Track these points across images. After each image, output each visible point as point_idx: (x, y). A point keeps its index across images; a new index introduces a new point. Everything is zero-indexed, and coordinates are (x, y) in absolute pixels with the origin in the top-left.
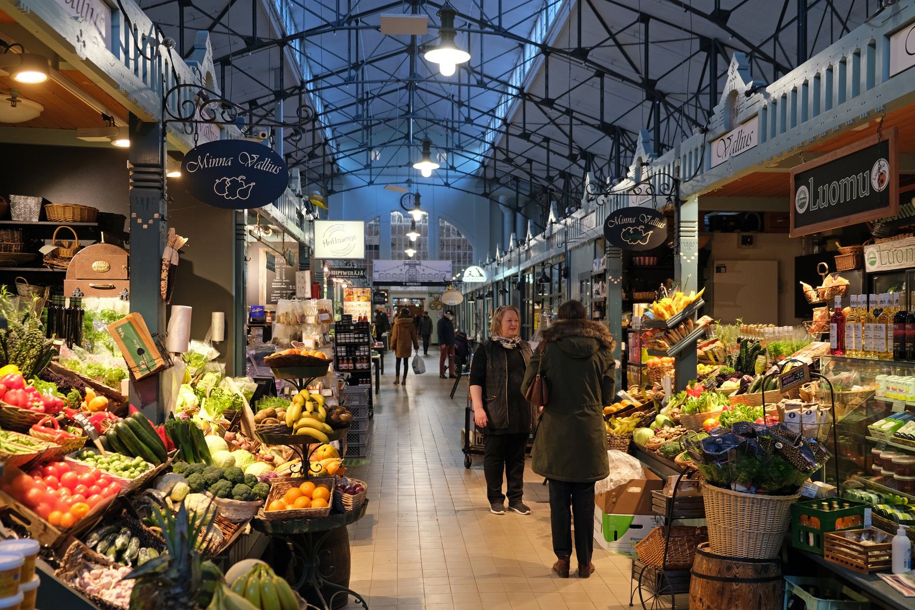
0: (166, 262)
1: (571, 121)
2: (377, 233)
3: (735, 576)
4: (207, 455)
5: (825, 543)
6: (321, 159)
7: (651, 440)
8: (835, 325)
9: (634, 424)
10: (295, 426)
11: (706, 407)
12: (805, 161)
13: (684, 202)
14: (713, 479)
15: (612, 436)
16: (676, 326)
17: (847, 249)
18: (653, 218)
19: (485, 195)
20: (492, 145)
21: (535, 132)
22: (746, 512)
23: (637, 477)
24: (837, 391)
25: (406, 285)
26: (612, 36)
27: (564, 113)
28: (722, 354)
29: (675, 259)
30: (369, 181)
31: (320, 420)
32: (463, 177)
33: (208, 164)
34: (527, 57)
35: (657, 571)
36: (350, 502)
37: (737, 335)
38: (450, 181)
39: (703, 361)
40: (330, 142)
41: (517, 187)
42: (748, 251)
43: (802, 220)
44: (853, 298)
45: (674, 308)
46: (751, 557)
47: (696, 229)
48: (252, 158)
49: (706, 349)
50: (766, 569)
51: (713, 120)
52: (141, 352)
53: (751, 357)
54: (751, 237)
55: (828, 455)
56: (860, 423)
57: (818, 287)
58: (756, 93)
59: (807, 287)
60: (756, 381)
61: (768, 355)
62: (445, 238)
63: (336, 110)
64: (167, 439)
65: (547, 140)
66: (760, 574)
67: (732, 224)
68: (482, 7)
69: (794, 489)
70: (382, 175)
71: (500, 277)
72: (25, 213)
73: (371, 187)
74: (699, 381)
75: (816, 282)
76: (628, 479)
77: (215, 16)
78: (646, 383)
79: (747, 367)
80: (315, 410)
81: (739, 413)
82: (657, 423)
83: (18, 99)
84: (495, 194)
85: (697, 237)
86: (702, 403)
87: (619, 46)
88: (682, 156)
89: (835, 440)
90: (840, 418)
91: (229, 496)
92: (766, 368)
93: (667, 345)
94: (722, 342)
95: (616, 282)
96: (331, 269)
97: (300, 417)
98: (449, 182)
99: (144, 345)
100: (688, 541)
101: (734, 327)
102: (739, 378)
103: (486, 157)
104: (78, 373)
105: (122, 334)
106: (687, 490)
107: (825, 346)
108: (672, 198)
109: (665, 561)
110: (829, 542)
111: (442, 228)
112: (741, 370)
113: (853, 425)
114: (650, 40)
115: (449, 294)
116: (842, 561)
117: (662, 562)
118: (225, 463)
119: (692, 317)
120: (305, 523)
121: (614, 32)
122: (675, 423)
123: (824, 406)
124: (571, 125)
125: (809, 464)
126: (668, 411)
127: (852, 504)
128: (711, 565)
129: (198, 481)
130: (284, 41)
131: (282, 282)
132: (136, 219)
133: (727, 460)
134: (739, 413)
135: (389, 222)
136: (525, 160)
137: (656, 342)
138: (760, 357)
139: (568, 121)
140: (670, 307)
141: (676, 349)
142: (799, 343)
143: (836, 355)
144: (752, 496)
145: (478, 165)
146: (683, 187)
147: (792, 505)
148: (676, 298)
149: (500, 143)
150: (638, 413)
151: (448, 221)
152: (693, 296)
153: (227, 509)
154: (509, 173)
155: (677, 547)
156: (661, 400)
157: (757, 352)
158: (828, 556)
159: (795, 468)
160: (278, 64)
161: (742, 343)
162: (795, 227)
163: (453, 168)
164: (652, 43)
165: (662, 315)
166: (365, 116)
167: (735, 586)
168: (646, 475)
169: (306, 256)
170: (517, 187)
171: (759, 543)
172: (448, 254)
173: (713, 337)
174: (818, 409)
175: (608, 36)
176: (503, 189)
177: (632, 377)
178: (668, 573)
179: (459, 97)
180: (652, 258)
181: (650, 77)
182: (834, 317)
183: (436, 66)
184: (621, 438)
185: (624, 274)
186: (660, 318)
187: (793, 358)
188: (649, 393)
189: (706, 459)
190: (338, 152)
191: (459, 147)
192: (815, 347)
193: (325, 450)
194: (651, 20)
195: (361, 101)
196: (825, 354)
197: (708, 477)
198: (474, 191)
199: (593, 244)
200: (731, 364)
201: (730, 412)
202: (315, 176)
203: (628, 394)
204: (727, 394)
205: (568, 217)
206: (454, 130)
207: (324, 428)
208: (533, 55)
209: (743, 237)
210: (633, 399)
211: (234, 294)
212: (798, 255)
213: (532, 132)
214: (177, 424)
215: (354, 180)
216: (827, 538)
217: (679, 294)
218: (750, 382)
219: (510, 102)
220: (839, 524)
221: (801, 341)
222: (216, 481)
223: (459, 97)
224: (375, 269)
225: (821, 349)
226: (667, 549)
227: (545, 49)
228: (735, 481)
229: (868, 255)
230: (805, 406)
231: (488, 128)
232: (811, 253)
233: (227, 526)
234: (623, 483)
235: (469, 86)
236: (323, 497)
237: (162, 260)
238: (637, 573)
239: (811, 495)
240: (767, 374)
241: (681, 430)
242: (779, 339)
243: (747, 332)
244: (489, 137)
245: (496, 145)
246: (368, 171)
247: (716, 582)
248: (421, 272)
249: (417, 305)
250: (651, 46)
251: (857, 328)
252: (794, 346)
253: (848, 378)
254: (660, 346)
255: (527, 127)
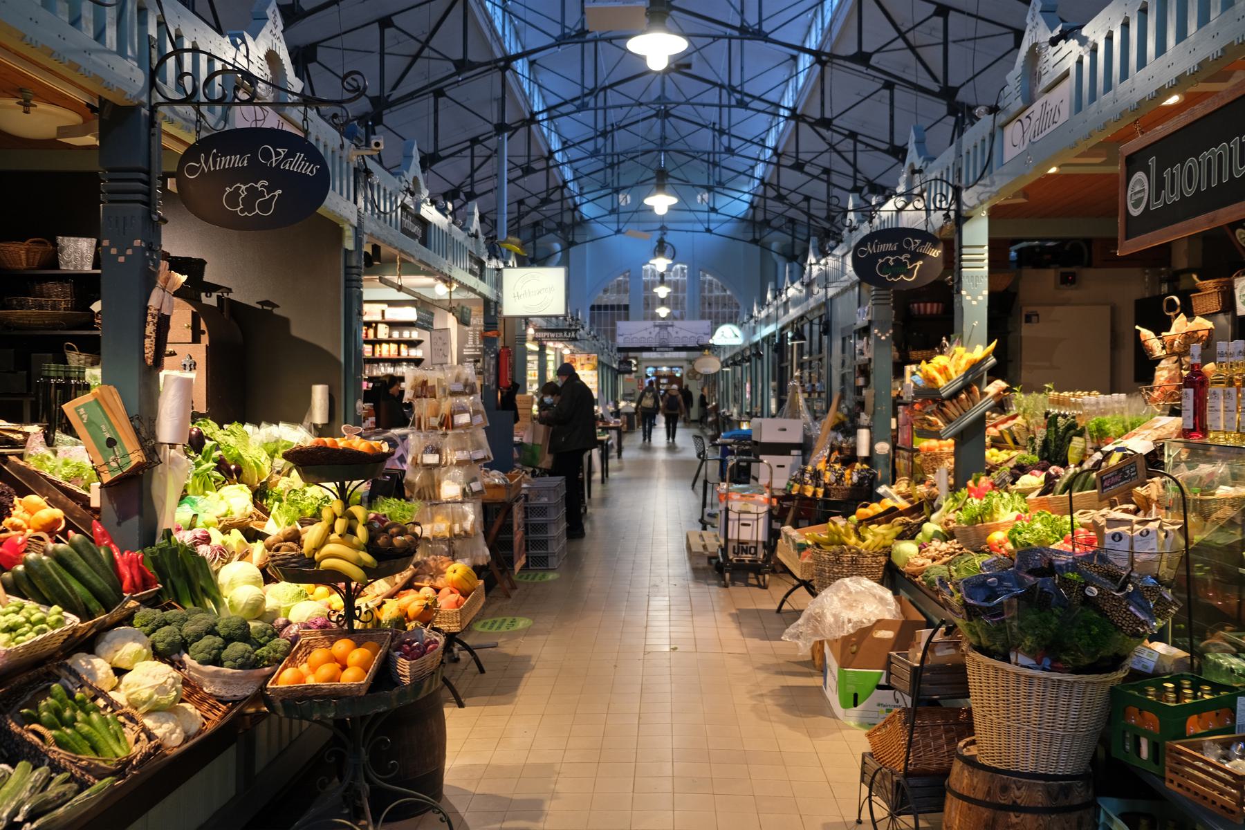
0: (152, 311)
1: (855, 146)
2: (626, 291)
3: (1014, 802)
4: (213, 593)
5: (1167, 759)
6: (558, 205)
7: (912, 561)
8: (1191, 391)
9: (893, 535)
10: (317, 556)
11: (991, 514)
12: (1142, 133)
13: (968, 218)
14: (980, 643)
15: (859, 553)
16: (954, 395)
17: (1210, 284)
18: (923, 243)
19: (755, 241)
20: (762, 180)
21: (809, 162)
22: (1034, 701)
23: (888, 617)
24: (1193, 495)
25: (655, 351)
26: (902, 35)
27: (847, 136)
28: (1023, 435)
29: (956, 300)
30: (616, 229)
31: (356, 548)
32: (728, 221)
33: (215, 166)
34: (801, 68)
35: (895, 778)
36: (407, 671)
37: (1044, 408)
38: (712, 226)
39: (999, 445)
40: (570, 185)
41: (793, 230)
42: (1069, 293)
43: (1135, 227)
44: (1221, 346)
45: (952, 370)
46: (1041, 771)
47: (986, 255)
48: (278, 154)
49: (1002, 427)
50: (1066, 791)
51: (1006, 94)
52: (111, 443)
53: (1062, 439)
54: (1073, 275)
55: (1176, 605)
56: (1230, 547)
57: (1164, 334)
58: (1067, 40)
59: (1146, 334)
60: (1068, 476)
61: (1088, 436)
62: (706, 294)
63: (574, 145)
64: (132, 577)
65: (827, 171)
66: (1056, 799)
67: (1047, 257)
68: (742, 11)
69: (1116, 662)
70: (633, 222)
71: (757, 338)
72: (75, 259)
73: (618, 236)
74: (988, 473)
75: (1161, 325)
76: (874, 619)
77: (423, 38)
78: (917, 476)
79: (1057, 454)
80: (351, 530)
81: (1038, 526)
82: (924, 535)
83: (32, 102)
84: (766, 240)
85: (986, 268)
86: (986, 509)
87: (912, 48)
88: (964, 154)
89: (1188, 570)
90: (1197, 538)
91: (217, 661)
92: (1085, 455)
93: (940, 424)
94: (1024, 418)
95: (883, 338)
96: (536, 331)
97: (324, 541)
98: (711, 228)
99: (115, 432)
100: (947, 732)
101: (1042, 396)
102: (1043, 470)
103: (754, 195)
104: (46, 472)
105: (85, 417)
106: (943, 654)
107: (1174, 423)
108: (952, 214)
109: (906, 764)
110: (1174, 758)
111: (704, 282)
112: (1048, 459)
113: (1218, 549)
114: (950, 38)
115: (703, 360)
116: (1196, 794)
117: (903, 765)
118: (246, 604)
119: (978, 382)
120: (329, 706)
121: (904, 29)
122: (948, 536)
123: (1171, 521)
124: (855, 151)
125: (1143, 623)
126: (940, 517)
127: (1216, 688)
128: (975, 780)
129: (169, 640)
130: (509, 60)
131: (475, 348)
132: (108, 249)
133: (1002, 614)
134: (1038, 526)
135: (640, 277)
136: (801, 197)
137: (925, 419)
138: (1076, 439)
139: (852, 147)
140: (946, 368)
141: (954, 429)
142: (1135, 419)
143: (1191, 440)
144: (1045, 674)
145: (746, 206)
146: (965, 195)
147: (1112, 688)
148: (955, 356)
149: (771, 177)
150: (900, 518)
151: (710, 274)
152: (980, 352)
153: (212, 682)
154: (782, 214)
155: (928, 740)
156: (934, 500)
157: (1072, 432)
158: (1172, 781)
159: (1119, 629)
160: (499, 93)
161: (1051, 420)
162: (1127, 238)
163: (713, 210)
164: (954, 42)
165: (932, 380)
166: (609, 150)
167: (1013, 818)
168: (903, 611)
169: (493, 313)
170: (793, 230)
171: (1055, 750)
172: (724, 314)
173: (1014, 410)
174: (1160, 527)
175: (896, 35)
176: (776, 234)
177: (902, 466)
178: (912, 782)
179: (720, 124)
180: (935, 305)
181: (951, 84)
182: (1188, 377)
183: (642, 59)
184: (874, 556)
185: (894, 326)
186: (931, 385)
187: (1119, 446)
188: (922, 489)
189: (968, 613)
190: (581, 195)
191: (721, 184)
192: (1158, 425)
193: (455, 572)
194: (952, 13)
195: (604, 134)
196: (1173, 439)
197: (974, 640)
198: (741, 236)
199: (857, 289)
200: (1034, 450)
201: (1026, 524)
202: (553, 225)
203: (892, 491)
204: (1024, 494)
205: (828, 255)
206: (715, 164)
207: (360, 559)
208: (808, 65)
209: (1062, 274)
210: (898, 498)
211: (342, 360)
212: (1139, 296)
213: (807, 162)
214: (174, 551)
215: (601, 230)
216: (1171, 750)
217: (959, 350)
218: (1058, 476)
219: (782, 125)
220: (1193, 725)
221: (1138, 415)
222: (199, 637)
223: (720, 124)
224: (619, 332)
225: (1168, 427)
226: (910, 744)
227: (817, 54)
228: (1016, 648)
229: (1241, 291)
230: (1139, 523)
231: (758, 159)
232: (1157, 294)
233: (213, 706)
234: (867, 624)
235: (730, 106)
236: (359, 664)
237: (147, 308)
238: (870, 778)
239: (1146, 667)
240: (1085, 466)
241: (957, 546)
242: (1104, 413)
243: (1058, 403)
244: (759, 171)
245: (766, 181)
246: (614, 217)
247: (982, 809)
248: (674, 335)
249: (678, 375)
250: (951, 47)
251: (1227, 395)
252: (1127, 424)
253: (1212, 474)
254: (930, 424)
255: (801, 156)
